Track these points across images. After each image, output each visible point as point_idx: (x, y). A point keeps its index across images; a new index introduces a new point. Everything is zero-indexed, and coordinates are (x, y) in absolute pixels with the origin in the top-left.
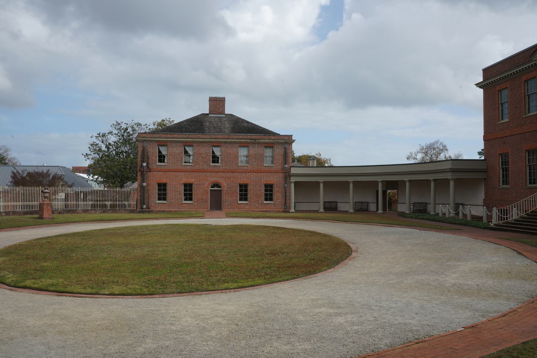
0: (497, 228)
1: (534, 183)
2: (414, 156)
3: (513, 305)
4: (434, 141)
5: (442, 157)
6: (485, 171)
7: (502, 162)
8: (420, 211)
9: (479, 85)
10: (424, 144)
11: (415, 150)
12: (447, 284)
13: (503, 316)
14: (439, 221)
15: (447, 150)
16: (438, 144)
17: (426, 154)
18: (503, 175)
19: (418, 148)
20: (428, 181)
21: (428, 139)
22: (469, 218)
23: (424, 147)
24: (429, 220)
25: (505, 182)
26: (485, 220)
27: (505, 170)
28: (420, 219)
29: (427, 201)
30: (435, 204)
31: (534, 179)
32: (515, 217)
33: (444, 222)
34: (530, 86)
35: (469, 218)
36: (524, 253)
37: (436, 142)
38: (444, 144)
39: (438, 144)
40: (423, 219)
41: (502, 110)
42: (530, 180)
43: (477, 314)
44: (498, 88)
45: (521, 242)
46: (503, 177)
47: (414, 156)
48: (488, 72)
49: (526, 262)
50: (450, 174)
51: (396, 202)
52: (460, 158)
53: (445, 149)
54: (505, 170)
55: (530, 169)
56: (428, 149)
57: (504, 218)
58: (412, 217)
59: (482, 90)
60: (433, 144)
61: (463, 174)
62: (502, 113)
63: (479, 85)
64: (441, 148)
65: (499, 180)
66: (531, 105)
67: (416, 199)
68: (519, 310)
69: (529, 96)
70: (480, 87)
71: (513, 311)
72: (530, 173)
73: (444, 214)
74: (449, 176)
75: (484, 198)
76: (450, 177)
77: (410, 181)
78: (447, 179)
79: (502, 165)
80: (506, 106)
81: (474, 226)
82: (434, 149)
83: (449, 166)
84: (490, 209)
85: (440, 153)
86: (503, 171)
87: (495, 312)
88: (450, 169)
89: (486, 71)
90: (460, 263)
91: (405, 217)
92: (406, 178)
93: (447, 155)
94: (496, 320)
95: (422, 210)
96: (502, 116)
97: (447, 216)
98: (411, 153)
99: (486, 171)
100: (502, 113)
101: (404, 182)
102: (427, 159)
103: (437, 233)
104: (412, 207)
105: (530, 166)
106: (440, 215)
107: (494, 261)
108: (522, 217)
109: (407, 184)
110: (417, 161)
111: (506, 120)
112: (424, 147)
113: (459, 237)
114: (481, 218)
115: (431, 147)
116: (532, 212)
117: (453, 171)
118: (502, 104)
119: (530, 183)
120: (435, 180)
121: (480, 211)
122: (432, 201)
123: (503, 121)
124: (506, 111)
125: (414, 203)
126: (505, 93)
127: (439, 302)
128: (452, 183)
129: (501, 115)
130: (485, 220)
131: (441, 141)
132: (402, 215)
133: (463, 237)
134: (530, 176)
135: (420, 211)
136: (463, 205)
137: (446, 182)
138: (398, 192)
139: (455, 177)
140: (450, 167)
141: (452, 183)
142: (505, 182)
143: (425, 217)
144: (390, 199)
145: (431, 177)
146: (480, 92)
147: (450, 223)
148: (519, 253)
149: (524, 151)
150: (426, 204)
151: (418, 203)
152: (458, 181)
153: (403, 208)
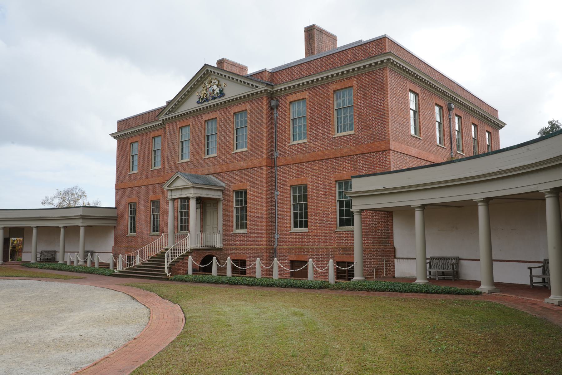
0: (122, 275)
1: (157, 231)
2: (50, 201)
3: (108, 351)
4: (73, 186)
5: (80, 203)
6: (115, 219)
7: (131, 211)
8: (48, 260)
9: (114, 136)
10: (61, 189)
11: (52, 195)
12: (49, 339)
13: (93, 366)
14: (65, 270)
15: (86, 196)
16: (77, 190)
17: (63, 199)
18: (131, 223)
19: (55, 193)
20: (58, 228)
21: (67, 183)
22: (96, 266)
23: (62, 192)
24: (56, 269)
25: (133, 230)
26: (111, 267)
27: (133, 218)
28: (45, 269)
29: (56, 249)
30: (64, 252)
31: (157, 227)
32: (138, 263)
33: (70, 271)
34: (156, 143)
35: (96, 266)
36: (137, 298)
37: (75, 188)
38: (83, 190)
39: (77, 190)
40: (49, 269)
41: (133, 162)
42: (154, 228)
43: (69, 368)
44: (130, 141)
45: (138, 287)
46: (131, 225)
47: (50, 201)
48: (122, 124)
49: (137, 306)
50: (81, 221)
51: (21, 250)
52: (98, 206)
53: (83, 195)
54: (133, 218)
55: (154, 218)
56: (63, 196)
57: (127, 264)
58: (36, 267)
59: (116, 141)
60: (72, 190)
61: (97, 222)
62: (133, 164)
63: (114, 136)
64: (80, 194)
65: (128, 228)
66: (156, 160)
67: (43, 247)
68: (112, 356)
69: (155, 151)
70: (114, 138)
71: (106, 358)
72: (154, 221)
73: (72, 263)
74: (79, 223)
75: (113, 245)
76: (80, 225)
77: (37, 227)
78: (30, 227)
79: (131, 214)
80: (136, 158)
81: (103, 272)
82: (72, 194)
83: (80, 212)
84: (116, 255)
85: (78, 200)
86: (131, 220)
87: (88, 362)
88: (81, 216)
89: (120, 123)
90: (72, 314)
91: (29, 267)
92: (33, 224)
93: (86, 202)
94: (84, 371)
95: (50, 259)
96: (133, 167)
97: (75, 264)
98: (47, 198)
99: (116, 219)
100: (133, 164)
101: (31, 229)
102: (65, 204)
103: (59, 283)
104: (39, 256)
105: (154, 215)
106: (68, 264)
107: (107, 309)
108: (143, 263)
109: (34, 231)
110: (53, 207)
111: (136, 171)
112: (62, 192)
113: (81, 286)
114: (107, 265)
115: (69, 192)
116: (152, 258)
117: (84, 218)
118: (133, 156)
119: (154, 231)
120: (65, 227)
121: (108, 258)
122: (61, 249)
123: (133, 172)
124: (136, 163)
125: (41, 252)
126: (136, 146)
127: (31, 361)
128: (82, 231)
129: (131, 166)
130: (111, 267)
131: (80, 187)
132: (27, 265)
133: (85, 286)
134: (154, 225)
135: (48, 260)
136: (92, 253)
137: (76, 229)
138: (23, 239)
139: (86, 224)
140: (81, 214)
141: (82, 231)
142: (133, 230)
143: (51, 267)
144: (14, 247)
145: (61, 224)
146: (114, 143)
147: (76, 272)
148: (133, 298)
149: (149, 201)
150: (55, 252)
151: (46, 252)
152: (88, 229)
153: (27, 257)
